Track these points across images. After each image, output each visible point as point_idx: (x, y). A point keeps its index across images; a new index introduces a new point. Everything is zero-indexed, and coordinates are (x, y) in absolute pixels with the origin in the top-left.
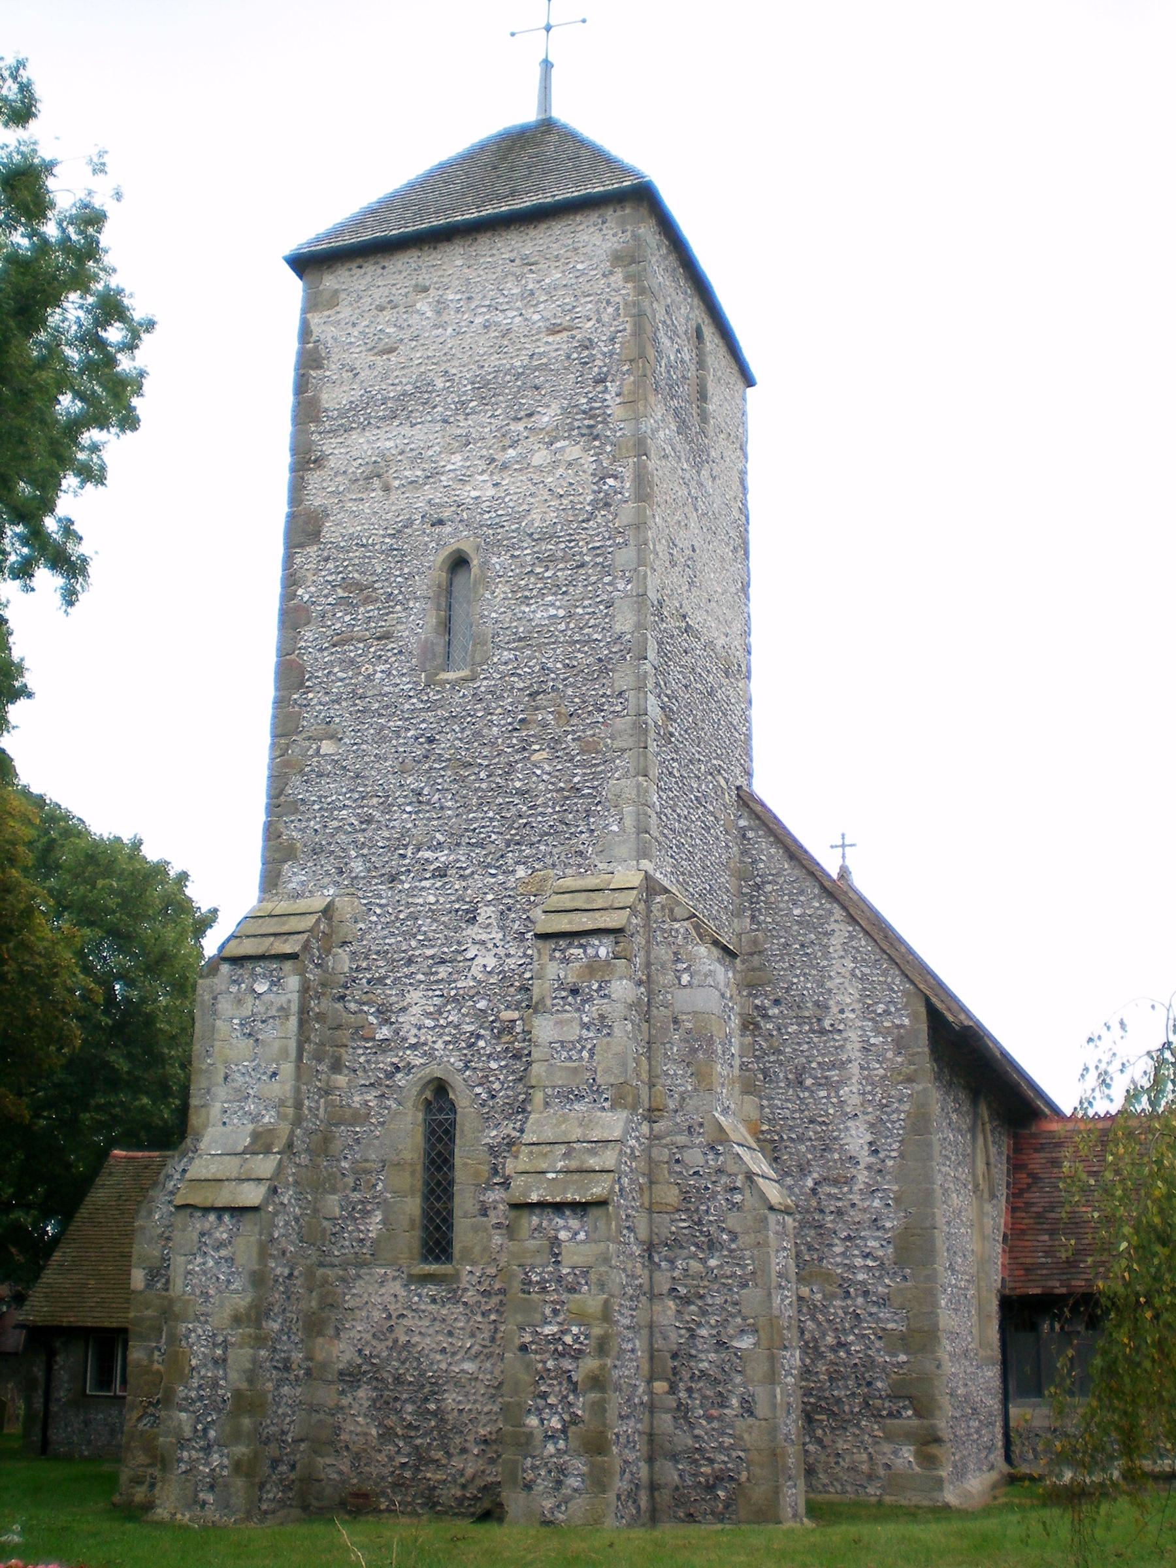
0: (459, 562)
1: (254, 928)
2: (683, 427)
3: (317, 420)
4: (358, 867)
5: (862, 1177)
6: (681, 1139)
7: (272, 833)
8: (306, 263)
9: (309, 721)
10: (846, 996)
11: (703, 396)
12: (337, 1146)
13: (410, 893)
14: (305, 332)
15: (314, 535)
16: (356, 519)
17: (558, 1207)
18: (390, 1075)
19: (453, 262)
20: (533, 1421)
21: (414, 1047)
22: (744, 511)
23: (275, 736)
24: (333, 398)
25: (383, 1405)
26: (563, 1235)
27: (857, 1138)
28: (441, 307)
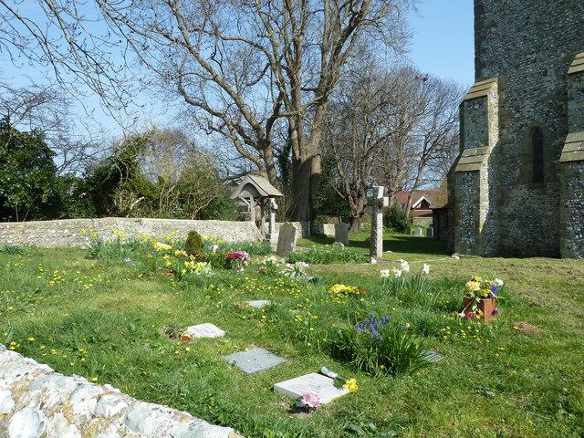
1: (475, 89)
4: (506, 65)
7: (477, 60)
9: (486, 23)
12: (505, 150)
13: (524, 70)
18: (521, 128)
20: (571, 228)
21: (527, 118)
23: (475, 30)
25: (522, 225)
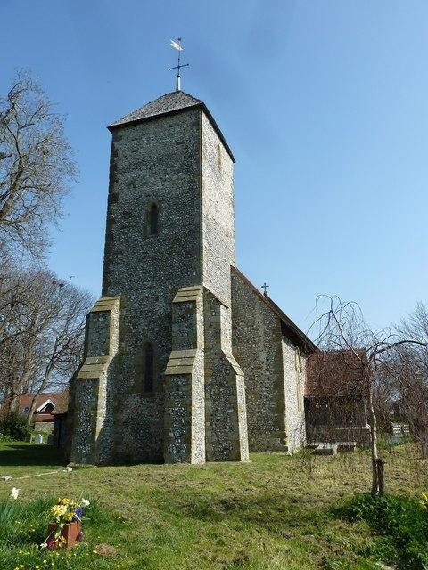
0: (154, 207)
2: (213, 170)
3: (116, 170)
5: (265, 366)
6: (213, 356)
7: (105, 279)
8: (112, 129)
9: (114, 249)
10: (259, 319)
11: (220, 163)
14: (113, 147)
15: (116, 201)
16: (126, 196)
17: (178, 375)
19: (152, 126)
22: (270, 300)
24: (121, 164)
26: (180, 383)
27: (263, 357)
28: (148, 139)
